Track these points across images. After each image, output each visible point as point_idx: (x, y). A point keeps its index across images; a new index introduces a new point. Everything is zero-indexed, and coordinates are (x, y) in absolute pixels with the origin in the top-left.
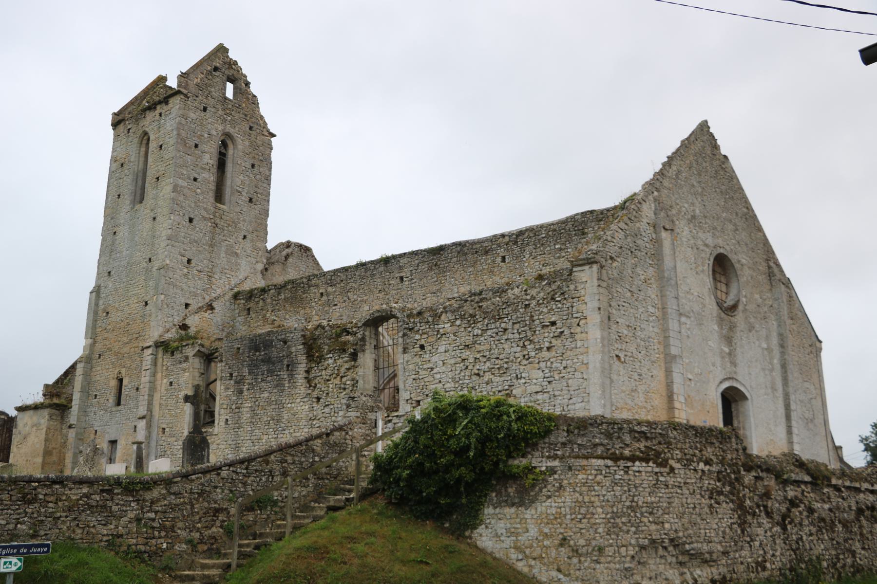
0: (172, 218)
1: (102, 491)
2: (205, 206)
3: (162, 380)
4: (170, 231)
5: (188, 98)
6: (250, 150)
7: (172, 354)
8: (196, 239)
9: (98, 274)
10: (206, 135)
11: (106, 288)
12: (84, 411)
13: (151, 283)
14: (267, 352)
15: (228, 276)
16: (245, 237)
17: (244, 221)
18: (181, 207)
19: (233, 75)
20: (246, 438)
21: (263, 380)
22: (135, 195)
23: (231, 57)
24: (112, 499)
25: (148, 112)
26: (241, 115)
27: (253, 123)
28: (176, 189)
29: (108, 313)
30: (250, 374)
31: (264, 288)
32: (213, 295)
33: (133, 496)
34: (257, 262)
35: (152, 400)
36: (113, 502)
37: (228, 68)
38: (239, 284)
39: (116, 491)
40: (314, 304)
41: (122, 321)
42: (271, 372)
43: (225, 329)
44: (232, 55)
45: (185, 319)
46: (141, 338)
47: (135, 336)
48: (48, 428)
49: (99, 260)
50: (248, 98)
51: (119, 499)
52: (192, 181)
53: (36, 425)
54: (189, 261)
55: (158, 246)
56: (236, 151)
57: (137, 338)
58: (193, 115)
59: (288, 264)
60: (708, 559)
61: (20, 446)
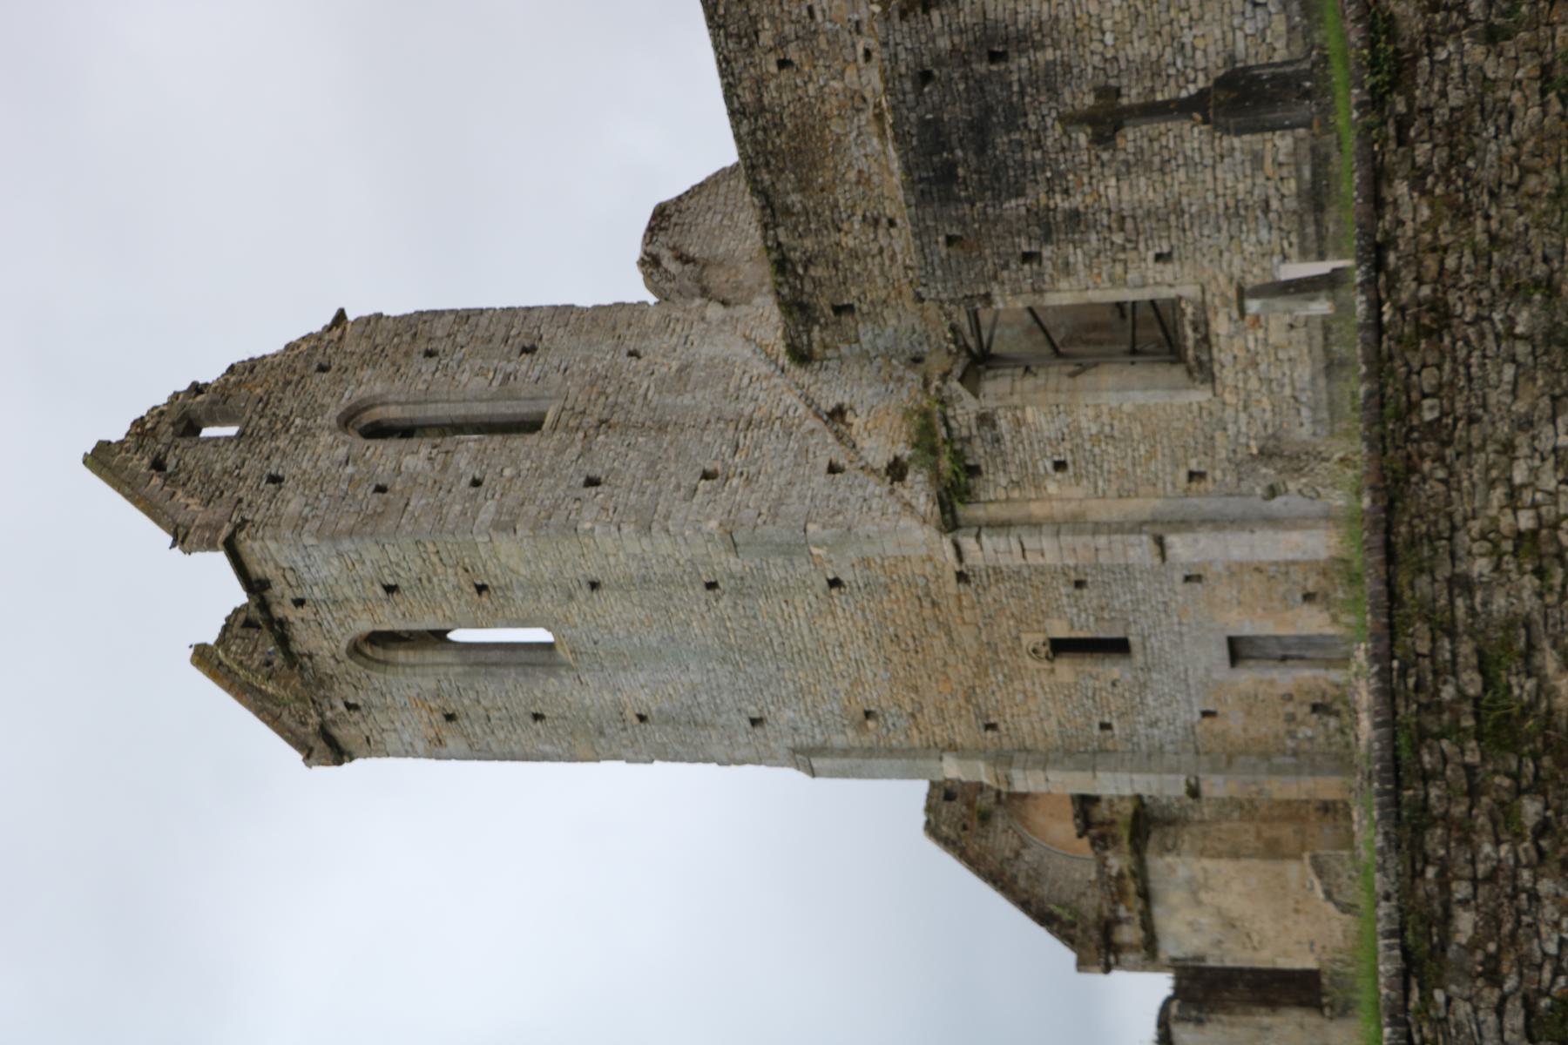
0: (588, 525)
1: (1402, 140)
2: (551, 453)
3: (1050, 498)
4: (625, 529)
5: (244, 521)
6: (387, 364)
7: (974, 471)
8: (644, 465)
9: (758, 761)
10: (350, 469)
11: (796, 729)
12: (1151, 758)
13: (776, 572)
14: (954, 137)
15: (746, 381)
16: (633, 354)
17: (587, 360)
18: (556, 507)
19: (173, 424)
20: (1210, 185)
21: (1039, 145)
22: (533, 665)
23: (121, 436)
24: (1429, 110)
25: (295, 647)
26: (289, 393)
27: (308, 364)
28: (505, 525)
29: (868, 714)
30: (1020, 193)
31: (775, 262)
32: (800, 411)
33: (1417, 57)
34: (703, 319)
35: (1109, 524)
36: (1436, 106)
37: (155, 437)
38: (767, 355)
39: (1401, 107)
40: (811, 89)
41: (888, 660)
42: (1014, 117)
43: (895, 375)
44: (117, 431)
45: (874, 471)
46: (933, 587)
47: (928, 612)
48: (1202, 853)
49: (721, 763)
50: (239, 384)
51: (1426, 95)
52: (482, 489)
53: (1195, 889)
54: (707, 476)
55: (671, 562)
56: (391, 398)
57: (934, 604)
58: (292, 506)
59: (706, 254)
60: (1448, 461)
61: (1255, 938)
